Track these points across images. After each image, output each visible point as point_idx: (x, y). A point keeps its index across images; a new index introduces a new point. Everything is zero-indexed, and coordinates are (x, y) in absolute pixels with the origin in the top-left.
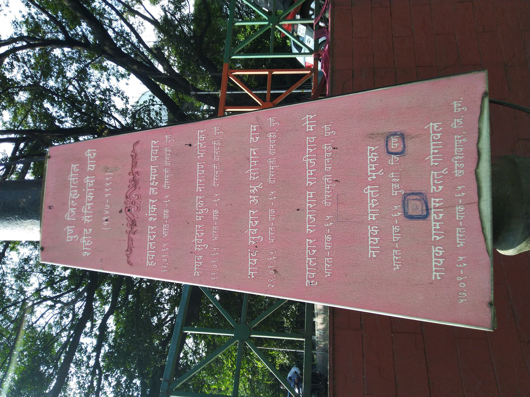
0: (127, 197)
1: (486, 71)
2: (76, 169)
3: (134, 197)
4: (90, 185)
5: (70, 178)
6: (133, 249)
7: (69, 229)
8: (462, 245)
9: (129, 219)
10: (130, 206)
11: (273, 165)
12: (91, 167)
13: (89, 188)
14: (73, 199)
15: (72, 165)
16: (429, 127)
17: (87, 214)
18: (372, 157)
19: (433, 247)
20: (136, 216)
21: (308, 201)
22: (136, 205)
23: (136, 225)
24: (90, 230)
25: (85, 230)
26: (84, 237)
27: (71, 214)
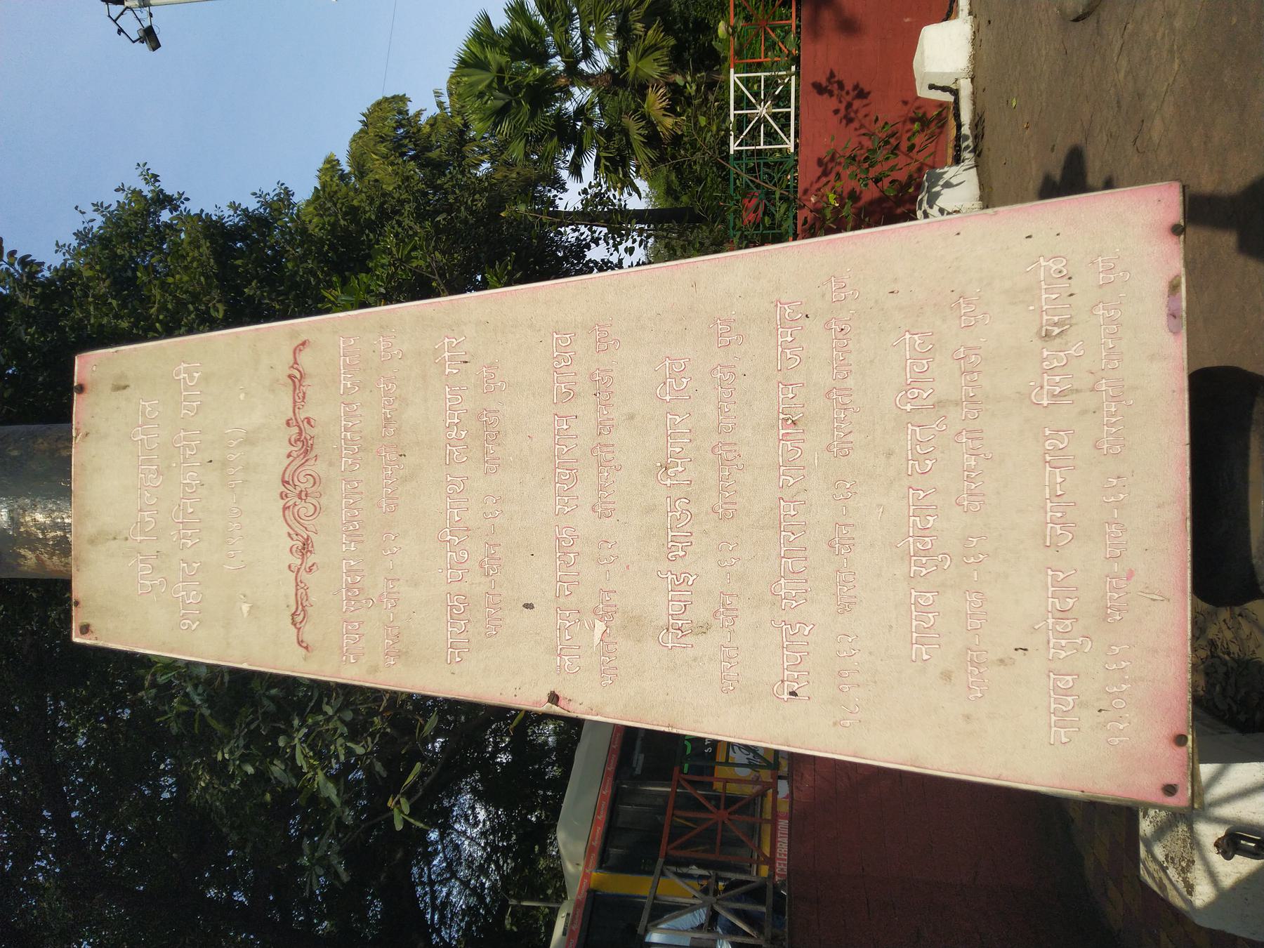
0: (285, 482)
1: (647, 940)
9: (294, 536)
20: (310, 528)
22: (309, 499)
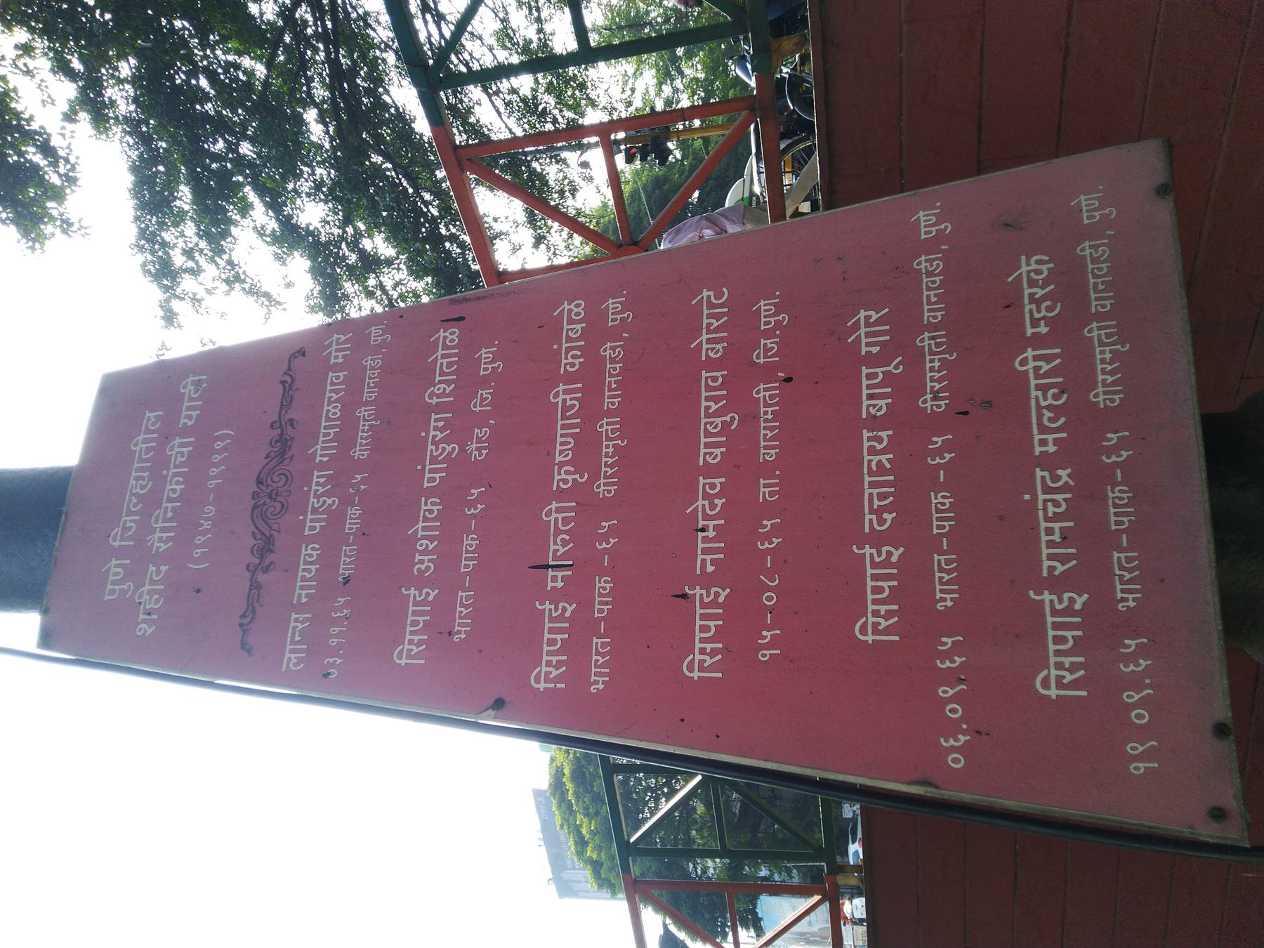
2: (153, 424)
3: (276, 479)
5: (136, 445)
7: (117, 566)
8: (1132, 604)
9: (258, 536)
10: (265, 504)
11: (612, 439)
13: (176, 467)
14: (137, 495)
16: (1021, 274)
17: (163, 530)
19: (1023, 258)
20: (275, 527)
23: (271, 551)
24: (163, 568)
25: (152, 568)
26: (147, 587)
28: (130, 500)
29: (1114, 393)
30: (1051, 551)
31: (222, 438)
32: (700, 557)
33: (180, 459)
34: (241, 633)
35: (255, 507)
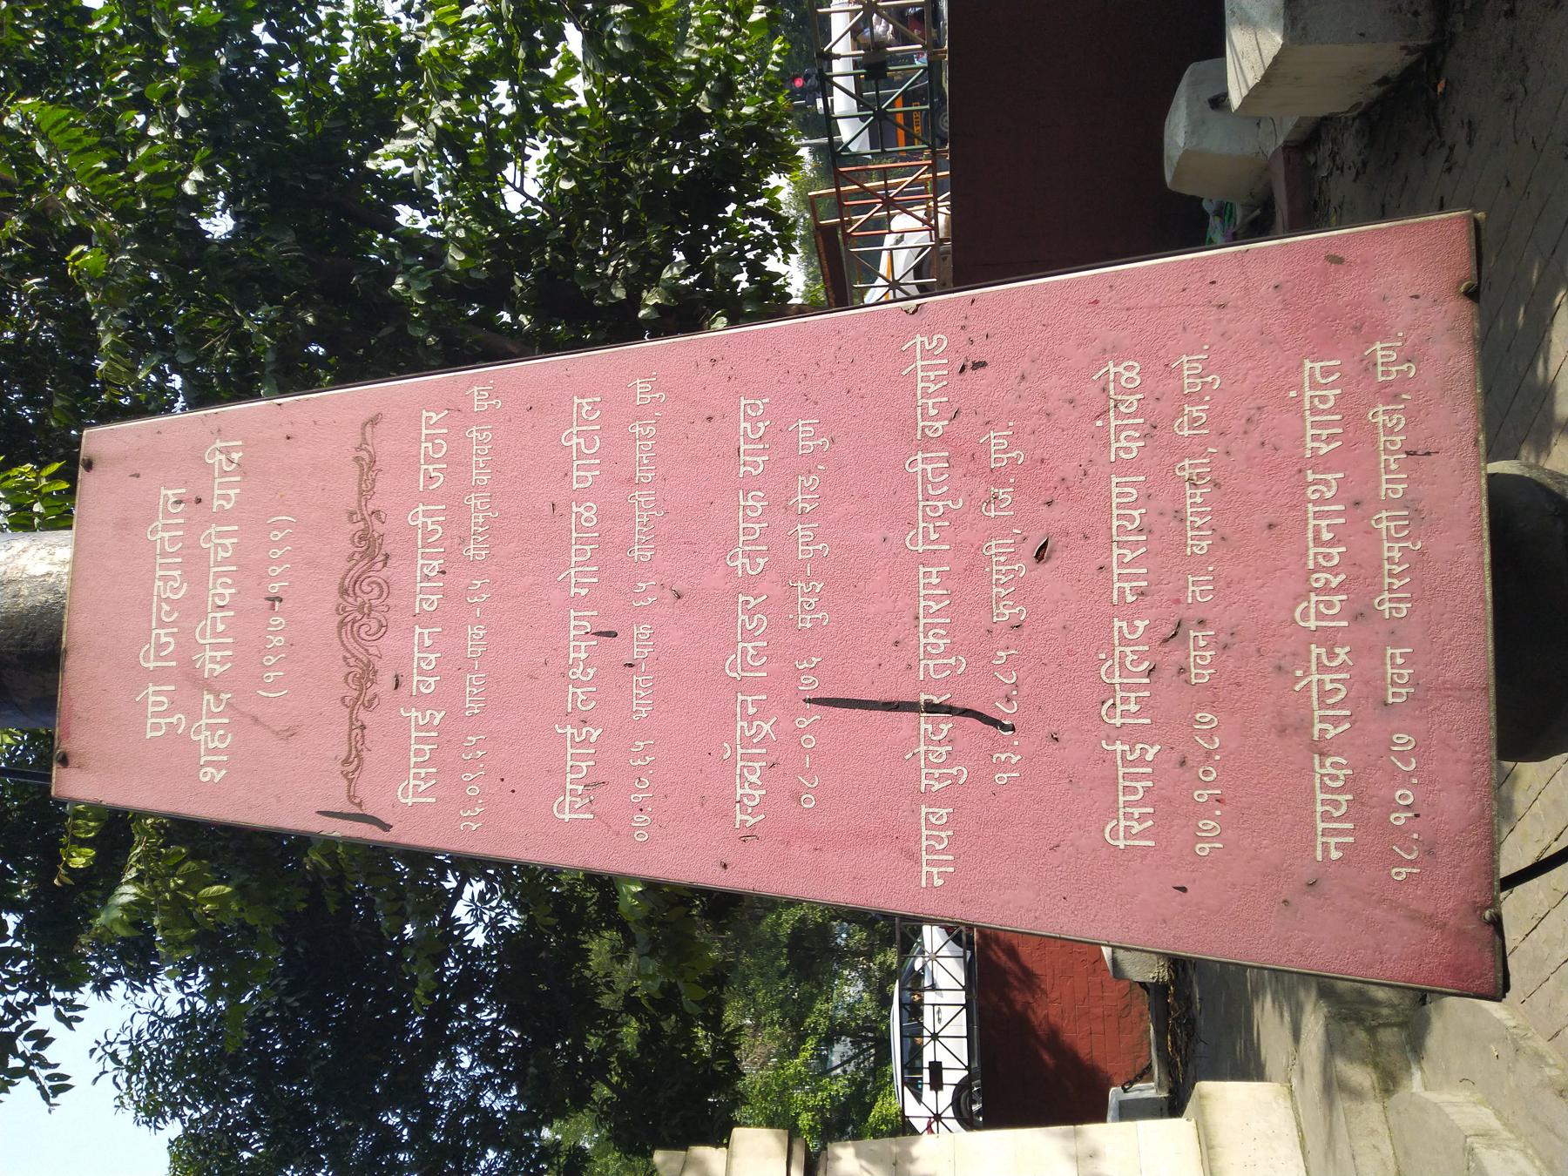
0: (343, 592)
3: (365, 588)
4: (221, 554)
6: (364, 754)
7: (156, 693)
9: (352, 661)
12: (226, 495)
15: (163, 492)
16: (1308, 686)
17: (216, 647)
18: (1124, 444)
20: (373, 650)
21: (922, 593)
27: (161, 646)
28: (160, 609)
29: (1400, 600)
30: (1322, 713)
31: (278, 527)
32: (1312, 522)
33: (221, 554)
34: (346, 783)
35: (342, 624)
